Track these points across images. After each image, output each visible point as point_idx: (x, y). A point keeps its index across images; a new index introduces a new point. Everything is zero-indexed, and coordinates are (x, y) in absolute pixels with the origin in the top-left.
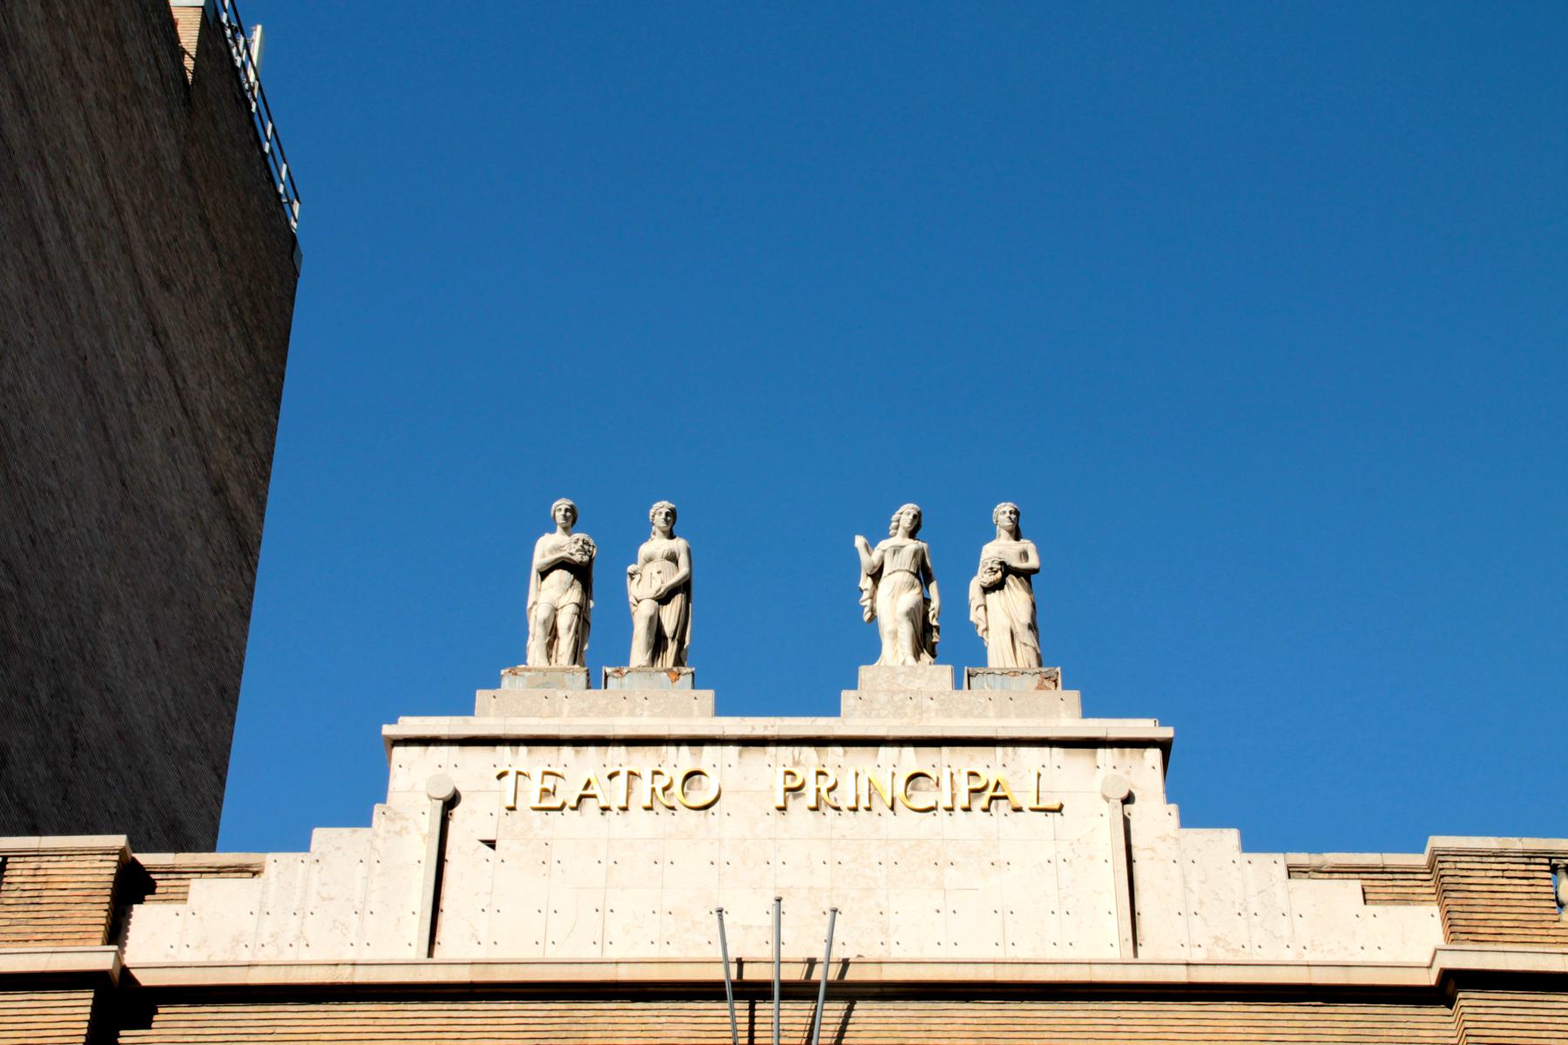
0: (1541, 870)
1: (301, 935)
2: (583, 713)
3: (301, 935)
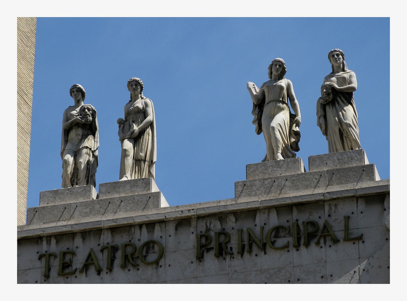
2: (87, 215)
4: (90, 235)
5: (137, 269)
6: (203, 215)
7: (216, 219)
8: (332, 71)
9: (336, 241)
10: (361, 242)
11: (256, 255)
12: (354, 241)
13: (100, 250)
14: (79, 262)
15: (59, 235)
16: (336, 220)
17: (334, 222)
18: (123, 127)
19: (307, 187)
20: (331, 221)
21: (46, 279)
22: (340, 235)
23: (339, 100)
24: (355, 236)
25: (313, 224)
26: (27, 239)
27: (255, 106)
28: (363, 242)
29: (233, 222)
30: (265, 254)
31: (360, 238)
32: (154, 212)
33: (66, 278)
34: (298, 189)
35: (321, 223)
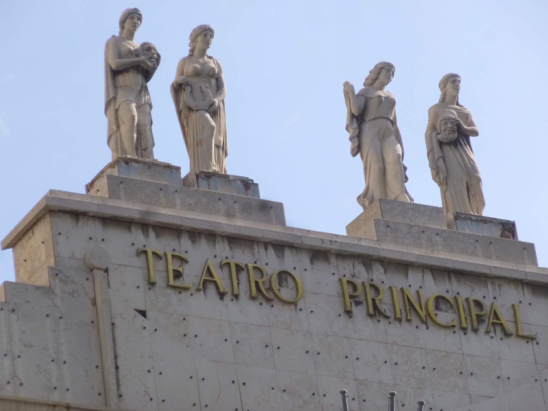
0: (92, 296)
1: (14, 375)
2: (191, 208)
3: (14, 375)
4: (200, 238)
5: (388, 322)
6: (109, 216)
7: (360, 263)
8: (186, 53)
9: (507, 335)
10: (535, 342)
11: (417, 327)
12: (180, 290)
13: (135, 254)
14: (192, 274)
15: (159, 226)
16: (503, 305)
17: (501, 307)
18: (192, 91)
19: (463, 252)
20: (497, 306)
21: (151, 287)
22: (510, 327)
23: (463, 143)
24: (526, 333)
25: (478, 304)
26: (116, 220)
27: (352, 116)
28: (538, 343)
29: (381, 273)
30: (427, 328)
31: (530, 339)
32: (277, 229)
33: (148, 288)
34: (452, 251)
35: (487, 303)
